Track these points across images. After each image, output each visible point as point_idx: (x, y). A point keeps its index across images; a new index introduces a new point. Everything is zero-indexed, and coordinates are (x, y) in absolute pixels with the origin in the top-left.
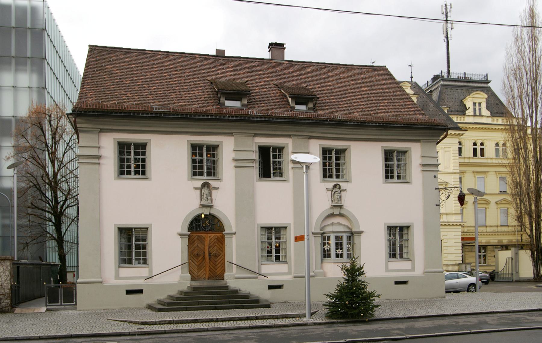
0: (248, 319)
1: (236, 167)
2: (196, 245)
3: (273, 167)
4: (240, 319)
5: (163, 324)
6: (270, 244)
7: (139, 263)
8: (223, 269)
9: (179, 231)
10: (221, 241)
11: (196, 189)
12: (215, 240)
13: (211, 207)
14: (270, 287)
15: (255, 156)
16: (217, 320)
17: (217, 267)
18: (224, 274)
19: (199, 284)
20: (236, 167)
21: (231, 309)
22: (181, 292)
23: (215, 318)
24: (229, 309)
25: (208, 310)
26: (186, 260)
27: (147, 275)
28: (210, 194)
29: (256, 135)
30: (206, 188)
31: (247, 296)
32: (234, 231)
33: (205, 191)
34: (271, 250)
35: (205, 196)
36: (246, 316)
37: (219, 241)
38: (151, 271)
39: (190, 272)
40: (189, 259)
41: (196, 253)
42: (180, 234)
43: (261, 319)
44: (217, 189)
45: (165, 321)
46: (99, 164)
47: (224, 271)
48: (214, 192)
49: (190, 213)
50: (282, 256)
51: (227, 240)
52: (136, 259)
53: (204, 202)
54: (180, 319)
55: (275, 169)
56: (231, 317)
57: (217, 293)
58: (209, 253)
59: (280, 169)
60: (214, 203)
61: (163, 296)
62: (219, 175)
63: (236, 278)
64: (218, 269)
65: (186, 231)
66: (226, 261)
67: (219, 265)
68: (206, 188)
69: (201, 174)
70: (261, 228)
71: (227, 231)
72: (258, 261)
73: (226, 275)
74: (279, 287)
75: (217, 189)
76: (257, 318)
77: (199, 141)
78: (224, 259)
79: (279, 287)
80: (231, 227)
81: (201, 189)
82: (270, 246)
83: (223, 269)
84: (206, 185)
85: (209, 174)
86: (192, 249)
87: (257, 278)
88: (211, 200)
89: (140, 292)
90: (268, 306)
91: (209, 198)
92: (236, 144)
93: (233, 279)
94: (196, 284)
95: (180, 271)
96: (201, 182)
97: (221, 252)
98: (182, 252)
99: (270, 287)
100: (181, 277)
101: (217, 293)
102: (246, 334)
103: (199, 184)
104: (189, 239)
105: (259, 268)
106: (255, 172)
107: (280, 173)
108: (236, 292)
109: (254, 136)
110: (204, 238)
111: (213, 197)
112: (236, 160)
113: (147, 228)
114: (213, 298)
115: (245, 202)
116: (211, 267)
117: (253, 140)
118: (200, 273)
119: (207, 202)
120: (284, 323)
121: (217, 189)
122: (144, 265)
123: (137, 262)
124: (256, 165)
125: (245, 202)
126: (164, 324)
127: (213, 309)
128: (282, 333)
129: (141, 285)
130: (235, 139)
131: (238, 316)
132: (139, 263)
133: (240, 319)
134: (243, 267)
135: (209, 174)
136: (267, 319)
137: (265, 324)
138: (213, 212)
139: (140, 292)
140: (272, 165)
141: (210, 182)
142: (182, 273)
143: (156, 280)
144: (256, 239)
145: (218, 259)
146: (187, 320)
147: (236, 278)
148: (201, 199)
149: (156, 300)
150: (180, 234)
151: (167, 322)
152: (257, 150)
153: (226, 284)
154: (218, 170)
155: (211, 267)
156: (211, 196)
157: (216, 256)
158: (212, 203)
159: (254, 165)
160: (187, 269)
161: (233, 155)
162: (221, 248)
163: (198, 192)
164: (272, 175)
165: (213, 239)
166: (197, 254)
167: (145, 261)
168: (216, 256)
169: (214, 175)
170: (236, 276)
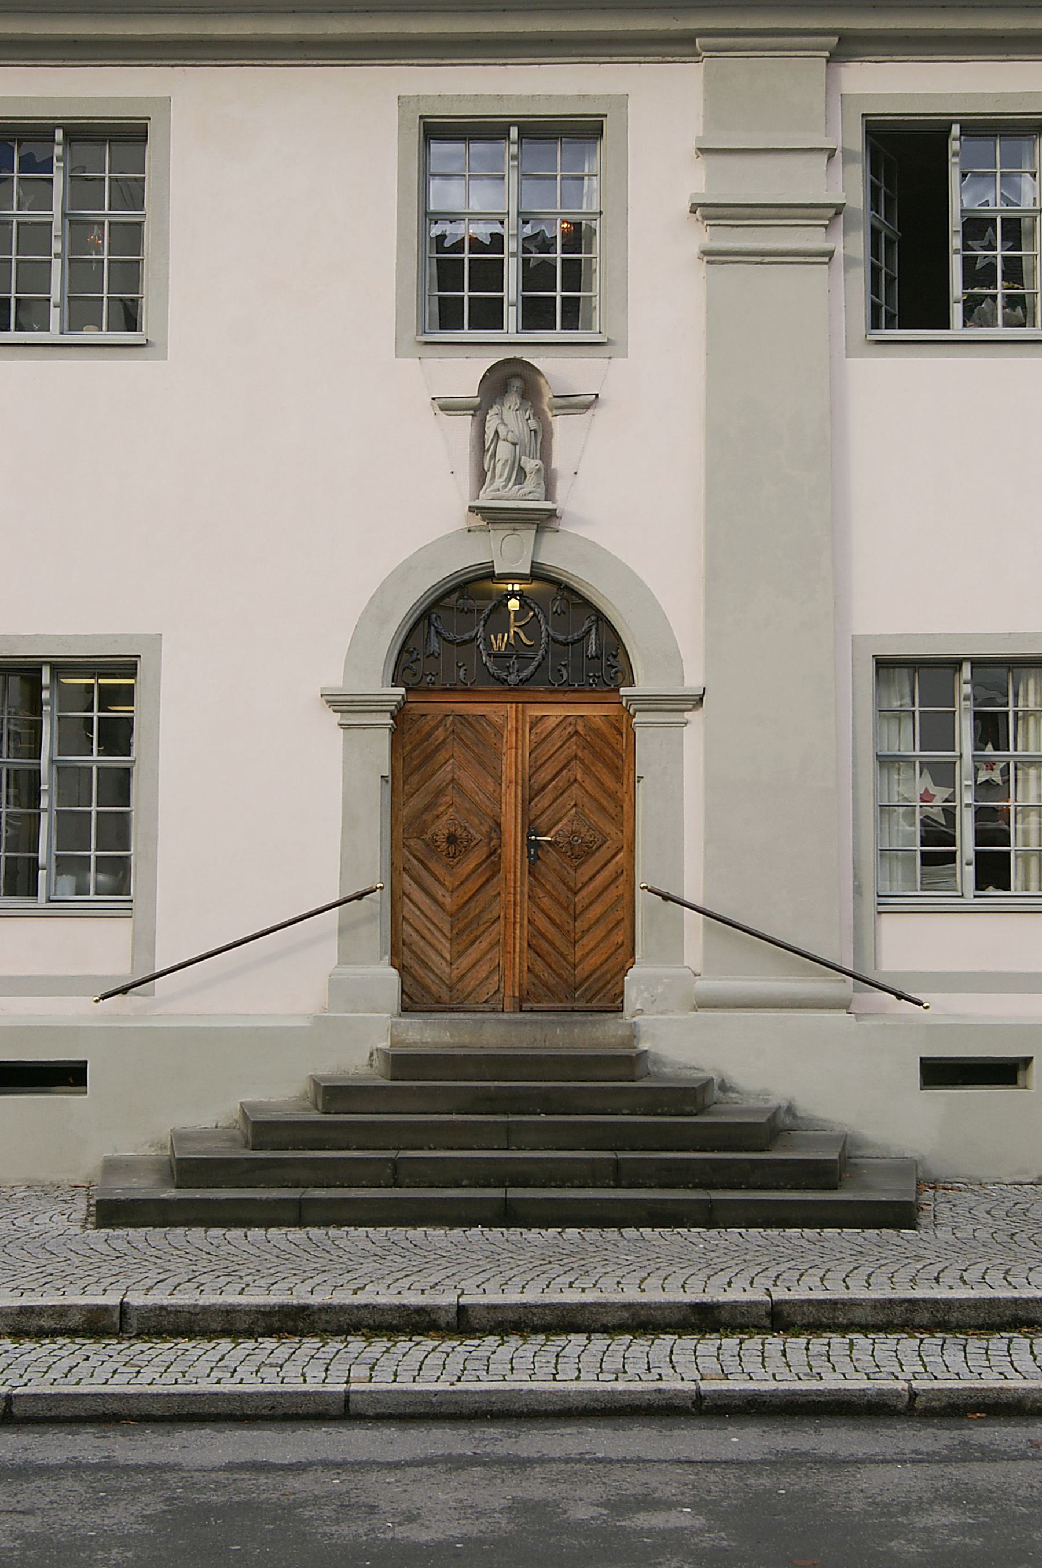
0: (704, 1320)
1: (711, 256)
2: (443, 775)
3: (968, 263)
4: (642, 1322)
5: (40, 1334)
6: (943, 774)
7: (81, 889)
8: (619, 937)
9: (336, 680)
10: (610, 756)
11: (448, 407)
12: (572, 748)
13: (542, 521)
14: (938, 1073)
15: (849, 185)
16: (463, 1323)
17: (581, 925)
18: (623, 971)
19: (447, 1037)
20: (711, 256)
21: (620, 1223)
22: (334, 1094)
23: (448, 1299)
24: (602, 1223)
25: (452, 1223)
26: (374, 870)
27: (121, 968)
28: (542, 442)
29: (848, 47)
30: (512, 401)
31: (774, 1127)
32: (692, 682)
33: (509, 418)
34: (949, 814)
35: (504, 451)
36: (694, 1295)
37: (598, 755)
38: (144, 942)
39: (399, 952)
40: (397, 869)
41: (441, 828)
42: (340, 704)
43: (816, 1328)
44: (587, 407)
45: (62, 1311)
46: (879, 896)
47: (625, 954)
48: (561, 425)
49: (407, 568)
50: (1026, 856)
51: (649, 744)
52: (63, 865)
53: (501, 493)
54: (184, 1298)
55: (978, 275)
56: (572, 1297)
57: (547, 1102)
58: (530, 827)
59: (1015, 271)
60: (564, 500)
61: (209, 1111)
62: (601, 324)
63: (705, 1004)
64: (588, 942)
65: (376, 681)
66: (640, 881)
67: (597, 910)
68: (512, 401)
69: (489, 315)
70: (884, 665)
71: (646, 681)
72: (858, 890)
73: (636, 984)
74: (1004, 1072)
75: (586, 404)
76: (778, 1319)
77: (460, 98)
78: (627, 872)
79: (1004, 1072)
80: (673, 659)
81: (479, 412)
82: (941, 793)
83: (619, 937)
84: (511, 381)
85: (536, 314)
86: (417, 802)
87: (844, 1005)
88: (548, 481)
89: (69, 1076)
90: (901, 1216)
91: (531, 464)
92: (714, 115)
93: (686, 1013)
94: (428, 1033)
95: (331, 948)
96: (481, 363)
97: (609, 828)
98: (350, 821)
99: (938, 1073)
100: (335, 985)
101: (547, 1102)
102: (633, 1482)
103: (465, 372)
104: (394, 732)
105: (862, 939)
106: (843, 288)
107: (1012, 301)
108: (693, 1094)
109: (834, 57)
110: (499, 733)
111: (558, 461)
112: (711, 212)
113: (129, 667)
114: (509, 1136)
115: (777, 493)
116: (543, 923)
117: (831, 82)
118: (465, 962)
119: (513, 490)
120: (991, 1382)
121: (586, 404)
122: (111, 902)
123: (68, 882)
124: (853, 245)
125: (777, 493)
126: (53, 1333)
127: (489, 1224)
128: (959, 1497)
129: (74, 1032)
130: (708, 79)
131: (632, 1295)
132: (81, 889)
133: (642, 1322)
134: (758, 937)
135: (536, 314)
136: (864, 1329)
137: (831, 1382)
138: (556, 556)
139: (69, 1076)
140: (956, 242)
141: (542, 361)
142: (344, 958)
143: (173, 1003)
144: (837, 729)
145: (587, 870)
146: (230, 1311)
147: (705, 1004)
148: (481, 477)
149: (165, 1136)
150: (340, 704)
151: (75, 1320)
152: (857, 142)
153: (633, 1037)
154: (598, 291)
155: (543, 923)
156: (545, 453)
157: (579, 851)
158: (549, 496)
159: (838, 243)
160: (375, 935)
161: (696, 182)
162: (611, 795)
163: (464, 425)
164: (957, 312)
165: (556, 740)
166: (452, 839)
167: (118, 876)
168: (579, 851)
169: (571, 321)
170: (705, 985)
